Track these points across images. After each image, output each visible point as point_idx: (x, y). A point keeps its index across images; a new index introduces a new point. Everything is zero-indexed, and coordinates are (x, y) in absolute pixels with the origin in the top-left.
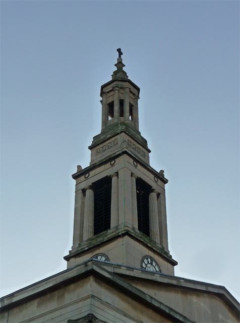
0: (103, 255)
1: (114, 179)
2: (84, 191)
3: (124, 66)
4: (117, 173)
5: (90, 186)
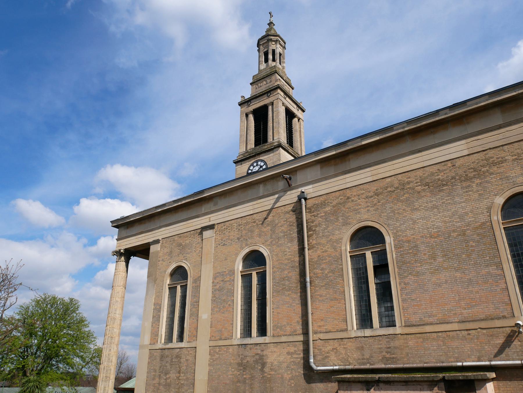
0: (262, 161)
2: (247, 115)
3: (274, 25)
4: (272, 104)
5: (252, 111)
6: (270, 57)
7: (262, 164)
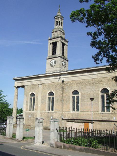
6: (58, 24)
7: (54, 61)
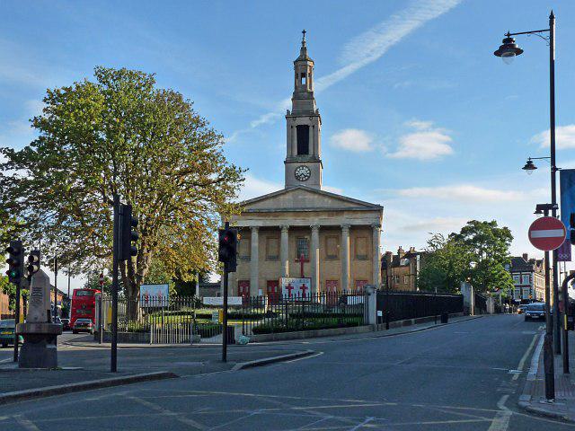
1: (311, 128)
